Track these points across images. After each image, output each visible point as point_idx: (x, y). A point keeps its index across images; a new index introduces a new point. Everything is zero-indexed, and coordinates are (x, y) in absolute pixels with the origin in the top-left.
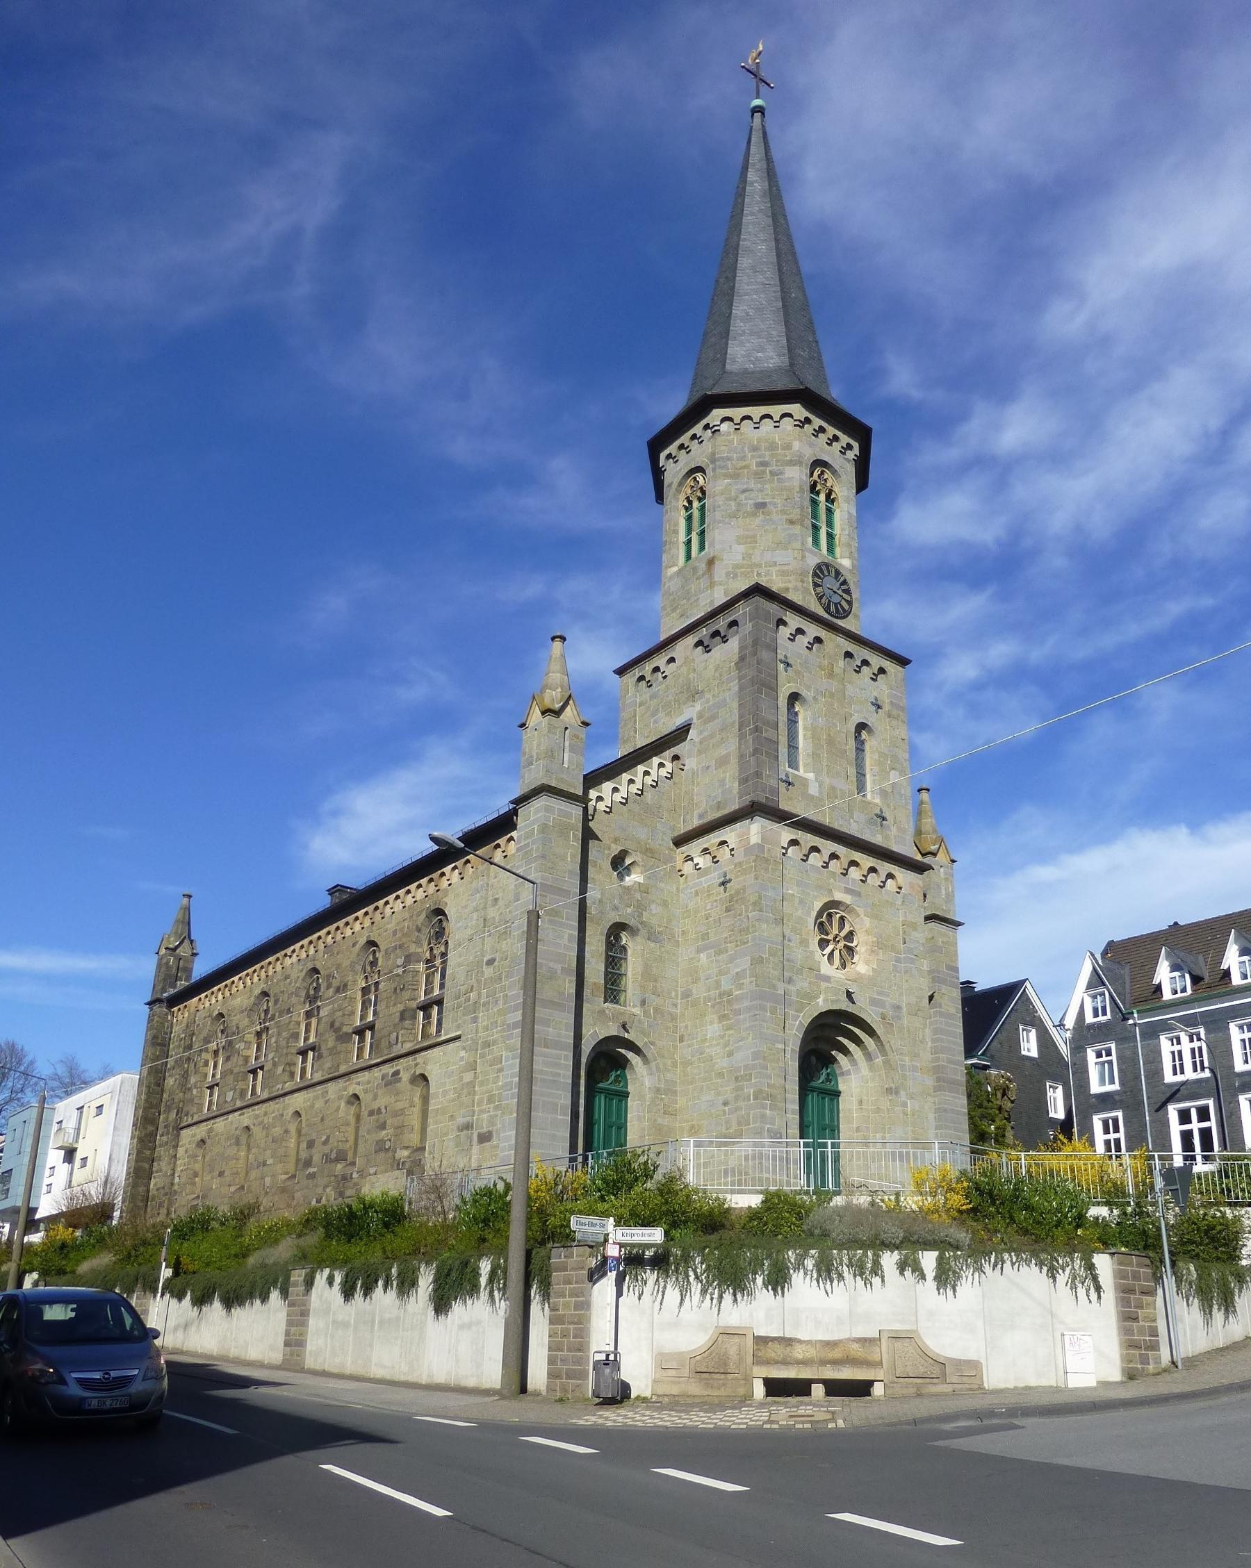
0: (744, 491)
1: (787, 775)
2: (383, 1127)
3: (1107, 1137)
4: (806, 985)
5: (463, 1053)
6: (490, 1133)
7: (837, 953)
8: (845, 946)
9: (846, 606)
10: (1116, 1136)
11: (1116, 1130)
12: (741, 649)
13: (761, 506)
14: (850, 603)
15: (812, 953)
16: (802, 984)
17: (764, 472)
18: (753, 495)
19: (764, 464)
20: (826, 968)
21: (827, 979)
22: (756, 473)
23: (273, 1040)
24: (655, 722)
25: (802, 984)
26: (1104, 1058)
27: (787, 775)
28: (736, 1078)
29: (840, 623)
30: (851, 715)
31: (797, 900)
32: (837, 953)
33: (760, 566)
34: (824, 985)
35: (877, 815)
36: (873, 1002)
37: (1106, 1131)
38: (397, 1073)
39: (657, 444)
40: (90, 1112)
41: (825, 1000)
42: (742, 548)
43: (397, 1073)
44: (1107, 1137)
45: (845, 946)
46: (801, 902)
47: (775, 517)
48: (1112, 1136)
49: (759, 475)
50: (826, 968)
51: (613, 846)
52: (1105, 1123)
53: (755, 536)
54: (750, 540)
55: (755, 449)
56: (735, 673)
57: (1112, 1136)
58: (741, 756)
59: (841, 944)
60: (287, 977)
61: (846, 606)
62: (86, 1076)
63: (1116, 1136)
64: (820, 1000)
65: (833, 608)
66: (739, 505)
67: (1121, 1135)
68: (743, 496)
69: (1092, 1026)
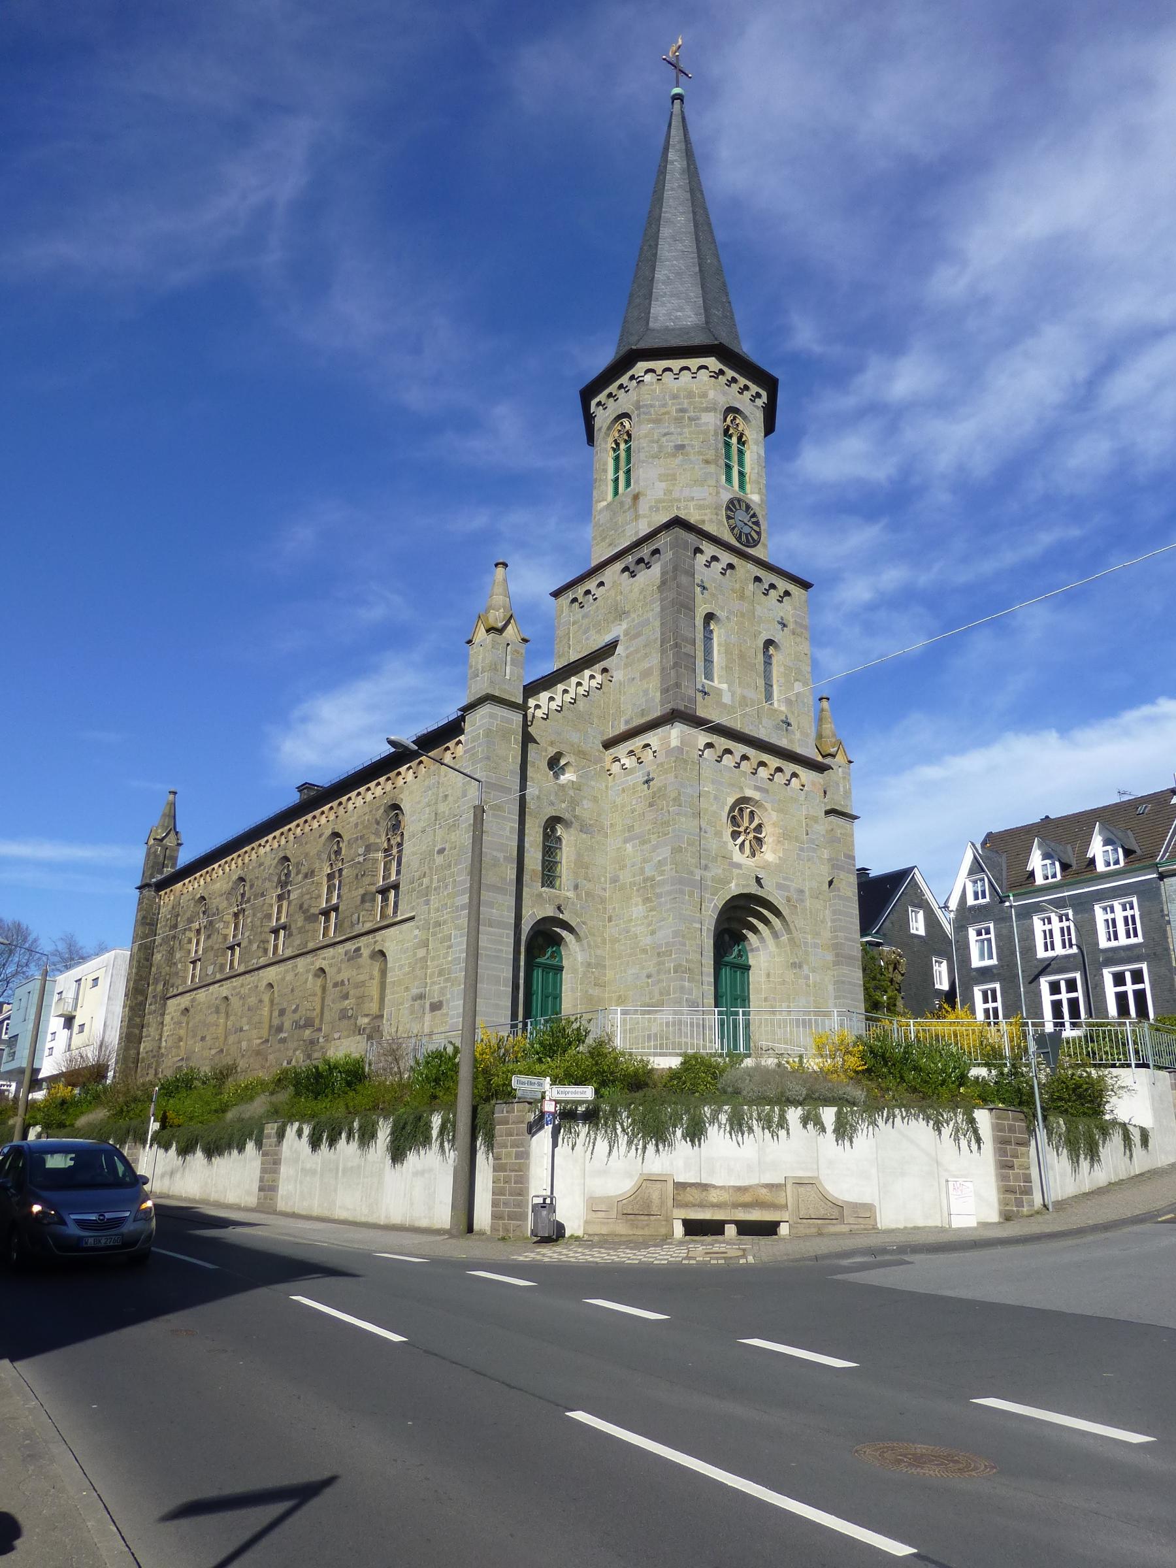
0: (665, 435)
1: (703, 686)
2: (346, 997)
3: (986, 1006)
4: (720, 871)
5: (416, 932)
6: (441, 1003)
7: (747, 843)
8: (755, 837)
9: (756, 537)
10: (995, 1005)
11: (995, 1000)
12: (663, 574)
13: (680, 448)
14: (759, 533)
15: (725, 843)
16: (716, 870)
17: (683, 418)
18: (673, 438)
19: (683, 410)
20: (738, 857)
21: (738, 866)
22: (676, 419)
23: (249, 920)
24: (587, 639)
25: (716, 870)
26: (984, 936)
27: (703, 686)
28: (659, 954)
29: (750, 551)
30: (760, 633)
31: (712, 796)
32: (747, 843)
33: (679, 500)
34: (736, 871)
35: (783, 722)
36: (780, 886)
37: (986, 1001)
38: (358, 949)
39: (588, 393)
40: (87, 983)
41: (737, 885)
42: (663, 485)
43: (358, 949)
44: (986, 1006)
45: (755, 837)
46: (716, 798)
47: (692, 457)
48: (991, 1005)
49: (678, 421)
50: (738, 857)
51: (550, 749)
52: (985, 994)
53: (674, 475)
54: (671, 478)
55: (675, 397)
56: (657, 596)
57: (991, 1005)
58: (663, 669)
59: (751, 836)
60: (260, 865)
61: (756, 537)
62: (84, 952)
63: (995, 1005)
64: (733, 885)
65: (744, 538)
66: (661, 447)
67: (999, 1004)
68: (664, 439)
69: (973, 908)
